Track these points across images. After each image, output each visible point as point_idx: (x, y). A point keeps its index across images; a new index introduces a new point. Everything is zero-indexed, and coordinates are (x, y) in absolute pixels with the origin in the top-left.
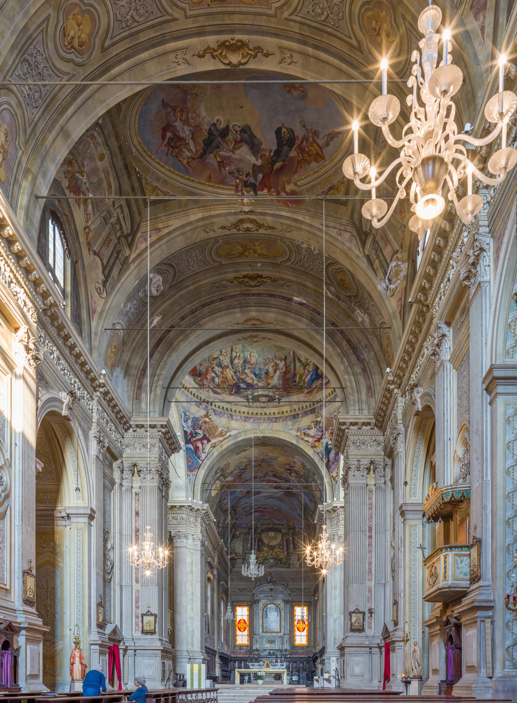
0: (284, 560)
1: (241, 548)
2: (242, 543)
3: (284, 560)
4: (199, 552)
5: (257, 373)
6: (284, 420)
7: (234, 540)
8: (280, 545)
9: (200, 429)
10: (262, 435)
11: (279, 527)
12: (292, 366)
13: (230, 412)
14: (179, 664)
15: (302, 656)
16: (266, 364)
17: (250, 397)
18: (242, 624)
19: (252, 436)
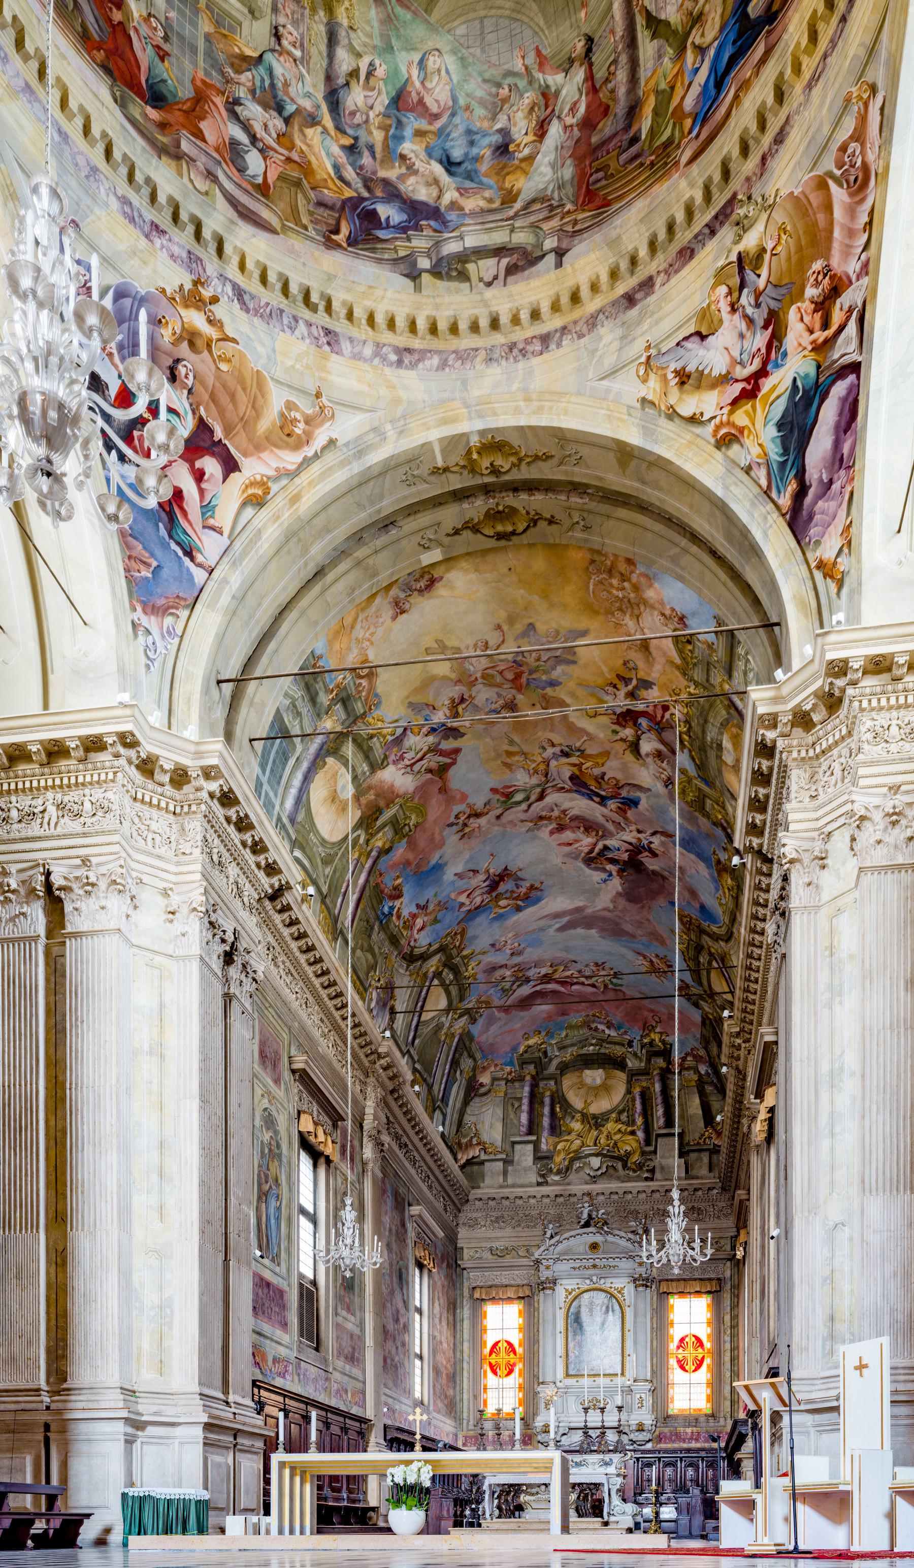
0: (636, 1158)
1: (499, 1127)
2: (500, 1112)
3: (636, 1158)
4: (195, 965)
5: (457, 154)
6: (581, 336)
7: (475, 1103)
8: (623, 1111)
10: (479, 425)
11: (618, 1050)
12: (622, 75)
13: (321, 319)
14: (83, 1447)
15: (694, 1445)
16: (497, 106)
17: (424, 263)
18: (503, 1354)
19: (434, 435)
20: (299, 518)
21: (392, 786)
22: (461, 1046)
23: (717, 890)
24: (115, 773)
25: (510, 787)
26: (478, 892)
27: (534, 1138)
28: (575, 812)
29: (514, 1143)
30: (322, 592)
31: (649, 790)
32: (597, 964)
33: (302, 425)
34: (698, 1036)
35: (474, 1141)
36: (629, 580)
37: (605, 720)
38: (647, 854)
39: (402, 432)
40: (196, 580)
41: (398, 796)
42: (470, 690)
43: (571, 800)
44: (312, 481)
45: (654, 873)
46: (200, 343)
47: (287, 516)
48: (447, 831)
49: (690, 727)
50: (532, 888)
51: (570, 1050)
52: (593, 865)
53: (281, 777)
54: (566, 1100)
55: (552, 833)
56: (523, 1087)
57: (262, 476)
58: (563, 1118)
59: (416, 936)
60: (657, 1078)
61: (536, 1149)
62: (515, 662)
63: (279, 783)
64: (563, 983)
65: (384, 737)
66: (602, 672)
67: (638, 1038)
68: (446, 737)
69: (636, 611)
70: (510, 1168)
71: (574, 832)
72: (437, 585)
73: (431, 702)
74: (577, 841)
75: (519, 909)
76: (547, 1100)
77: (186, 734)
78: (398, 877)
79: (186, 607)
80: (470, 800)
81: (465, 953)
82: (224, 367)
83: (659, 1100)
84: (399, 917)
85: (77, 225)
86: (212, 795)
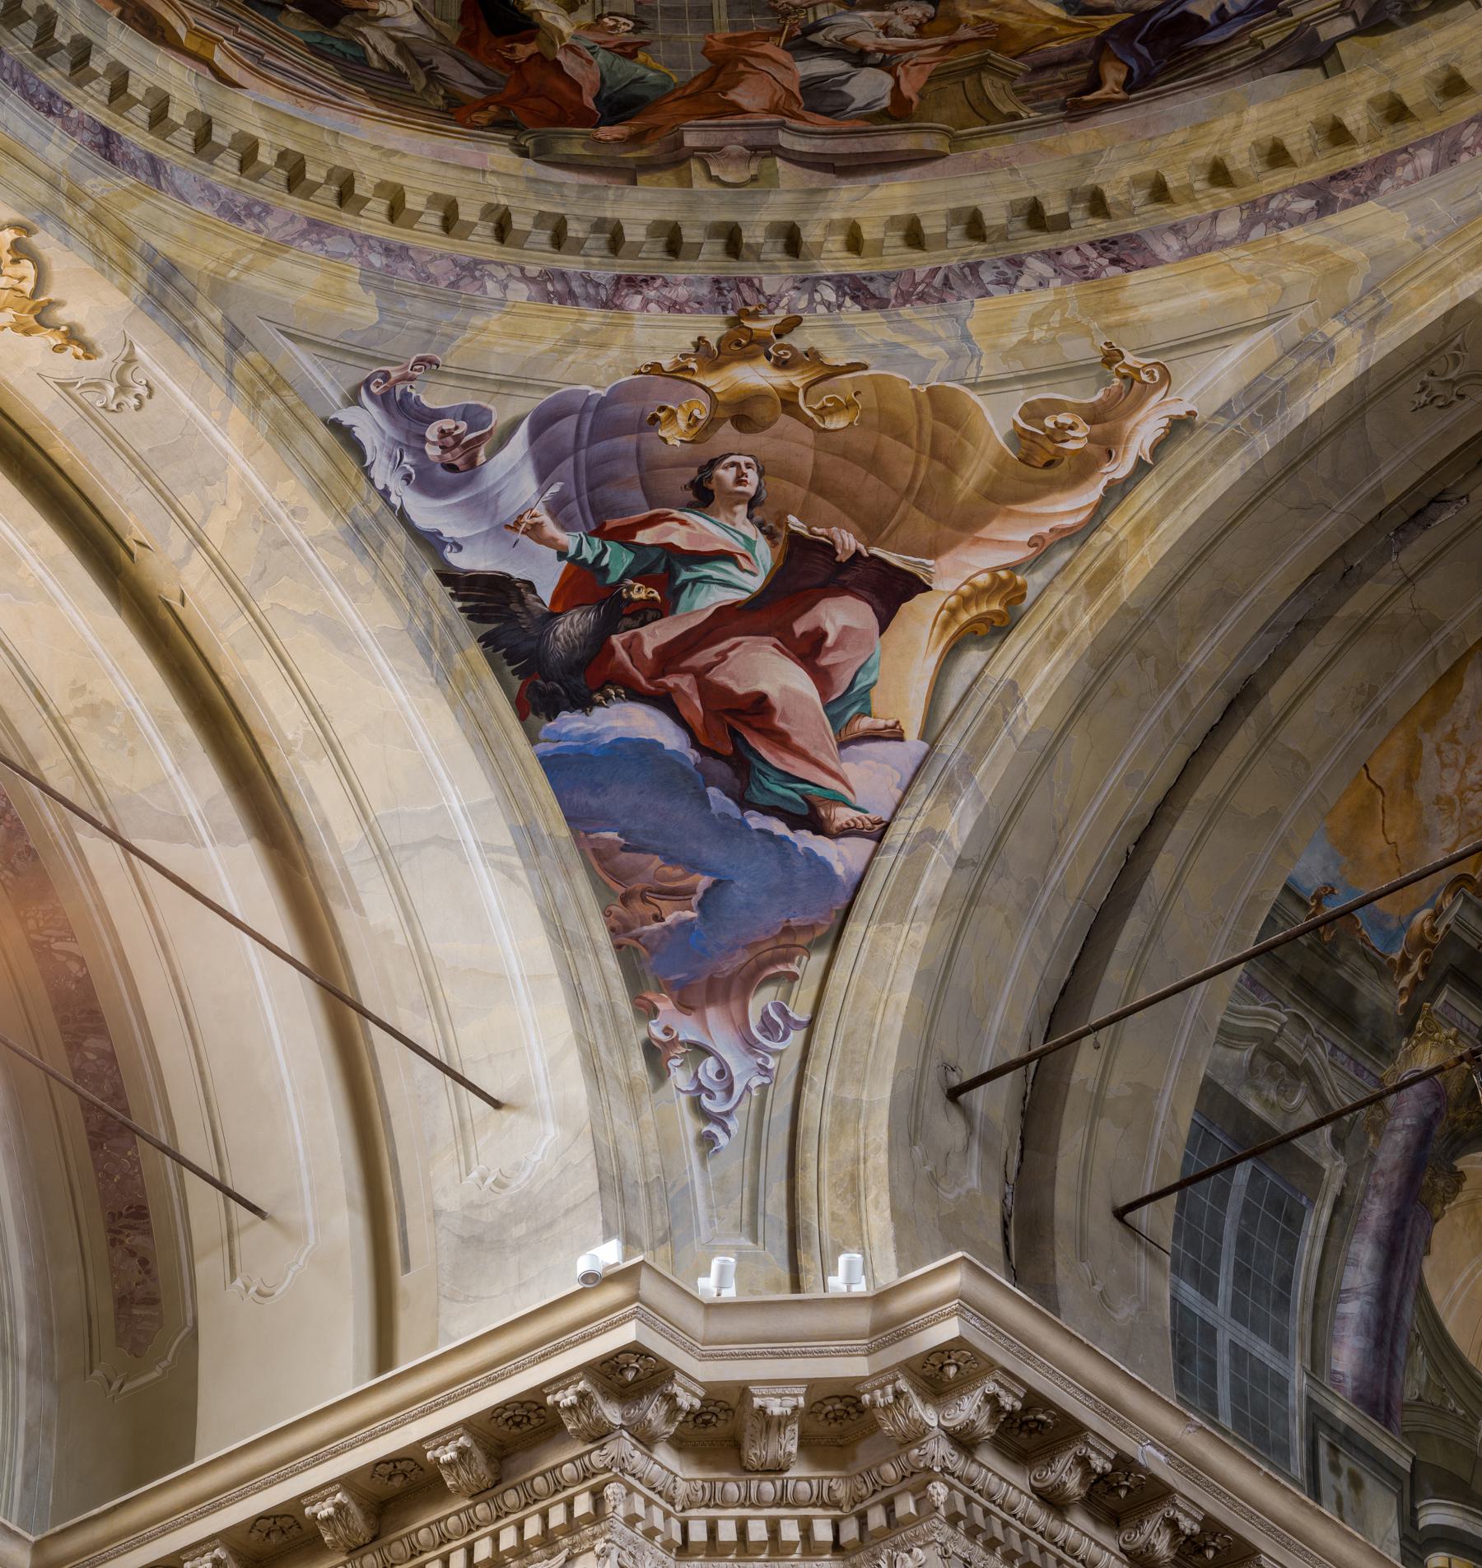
9: (703, 496)
20: (1125, 609)
24: (597, 1496)
30: (1265, 740)
33: (1082, 431)
39: (1375, 320)
40: (839, 870)
44: (1145, 519)
46: (761, 411)
47: (1086, 623)
53: (1286, 1282)
57: (993, 572)
63: (1283, 1302)
77: (837, 1284)
79: (817, 944)
82: (837, 422)
85: (431, 362)
86: (963, 1441)
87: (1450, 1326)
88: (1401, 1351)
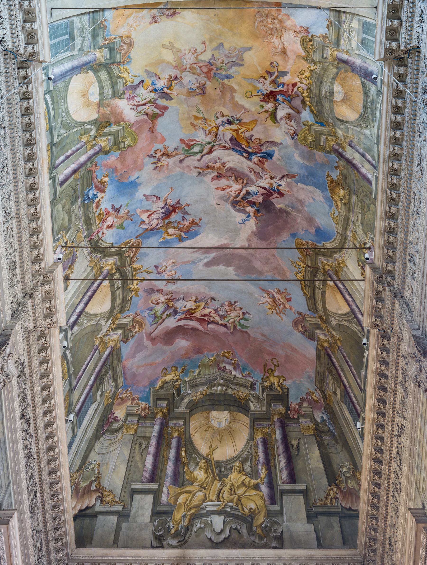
0: (261, 519)
2: (126, 452)
7: (105, 439)
11: (243, 392)
21: (122, 112)
22: (110, 362)
23: (330, 207)
25: (192, 141)
26: (156, 216)
27: (155, 486)
28: (229, 165)
29: (134, 491)
31: (281, 144)
32: (230, 304)
34: (313, 375)
35: (93, 488)
36: (277, 18)
37: (256, 99)
38: (276, 195)
41: (123, 120)
42: (182, 74)
43: (229, 155)
45: (281, 210)
48: (147, 160)
49: (311, 90)
50: (193, 222)
51: (200, 389)
52: (238, 208)
54: (192, 443)
55: (213, 179)
56: (154, 424)
58: (187, 464)
59: (105, 231)
60: (277, 424)
61: (156, 500)
62: (209, 62)
64: (201, 321)
65: (127, 82)
66: (258, 70)
67: (260, 381)
68: (162, 98)
69: (280, 34)
70: (124, 525)
71: (228, 180)
72: (176, 15)
73: (158, 74)
74: (229, 187)
75: (181, 239)
76: (174, 442)
78: (106, 176)
80: (166, 143)
81: (135, 265)
83: (281, 449)
84: (97, 206)
87: (70, 86)
88: (62, 80)
